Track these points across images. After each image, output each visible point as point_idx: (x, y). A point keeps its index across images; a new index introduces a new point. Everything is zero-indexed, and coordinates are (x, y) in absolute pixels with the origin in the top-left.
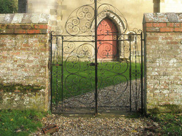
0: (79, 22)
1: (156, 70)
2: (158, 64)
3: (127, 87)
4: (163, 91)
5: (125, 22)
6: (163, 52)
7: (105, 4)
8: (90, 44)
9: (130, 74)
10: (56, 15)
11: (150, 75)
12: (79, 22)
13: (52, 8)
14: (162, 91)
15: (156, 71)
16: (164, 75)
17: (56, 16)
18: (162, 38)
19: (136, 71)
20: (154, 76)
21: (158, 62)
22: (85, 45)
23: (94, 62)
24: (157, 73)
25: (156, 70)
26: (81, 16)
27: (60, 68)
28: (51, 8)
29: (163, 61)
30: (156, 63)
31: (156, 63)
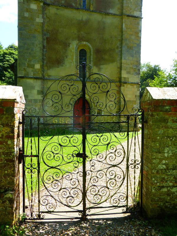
0: (62, 97)
1: (164, 162)
2: (166, 155)
3: (123, 182)
4: (172, 189)
5: (123, 98)
6: (173, 139)
7: (97, 74)
8: (122, 161)
9: (127, 164)
10: (42, 94)
11: (156, 169)
12: (62, 97)
13: (39, 89)
14: (170, 189)
15: (164, 164)
16: (173, 169)
17: (42, 95)
18: (173, 120)
19: (135, 162)
20: (162, 170)
21: (166, 151)
22: (123, 153)
23: (81, 152)
24: (164, 166)
25: (164, 162)
26: (96, 150)
27: (35, 159)
28: (38, 89)
29: (172, 151)
30: (164, 153)
31: (164, 153)
